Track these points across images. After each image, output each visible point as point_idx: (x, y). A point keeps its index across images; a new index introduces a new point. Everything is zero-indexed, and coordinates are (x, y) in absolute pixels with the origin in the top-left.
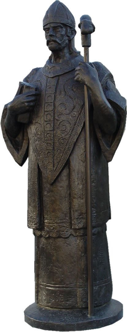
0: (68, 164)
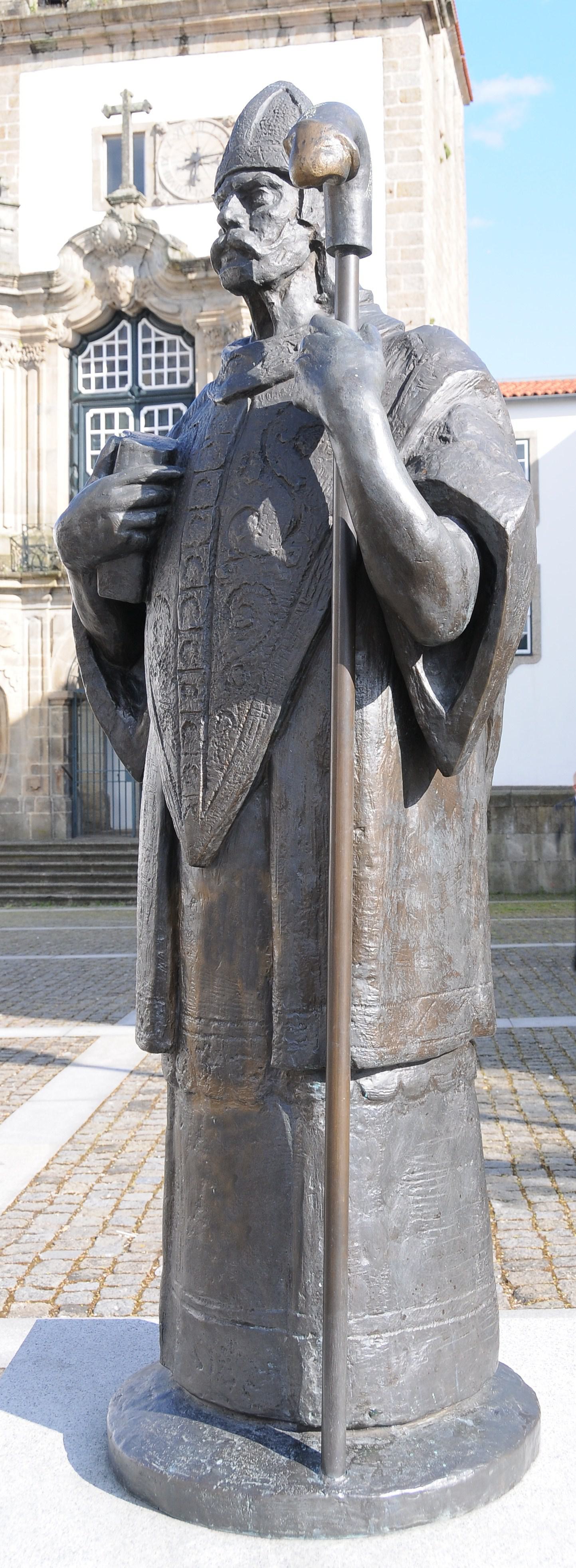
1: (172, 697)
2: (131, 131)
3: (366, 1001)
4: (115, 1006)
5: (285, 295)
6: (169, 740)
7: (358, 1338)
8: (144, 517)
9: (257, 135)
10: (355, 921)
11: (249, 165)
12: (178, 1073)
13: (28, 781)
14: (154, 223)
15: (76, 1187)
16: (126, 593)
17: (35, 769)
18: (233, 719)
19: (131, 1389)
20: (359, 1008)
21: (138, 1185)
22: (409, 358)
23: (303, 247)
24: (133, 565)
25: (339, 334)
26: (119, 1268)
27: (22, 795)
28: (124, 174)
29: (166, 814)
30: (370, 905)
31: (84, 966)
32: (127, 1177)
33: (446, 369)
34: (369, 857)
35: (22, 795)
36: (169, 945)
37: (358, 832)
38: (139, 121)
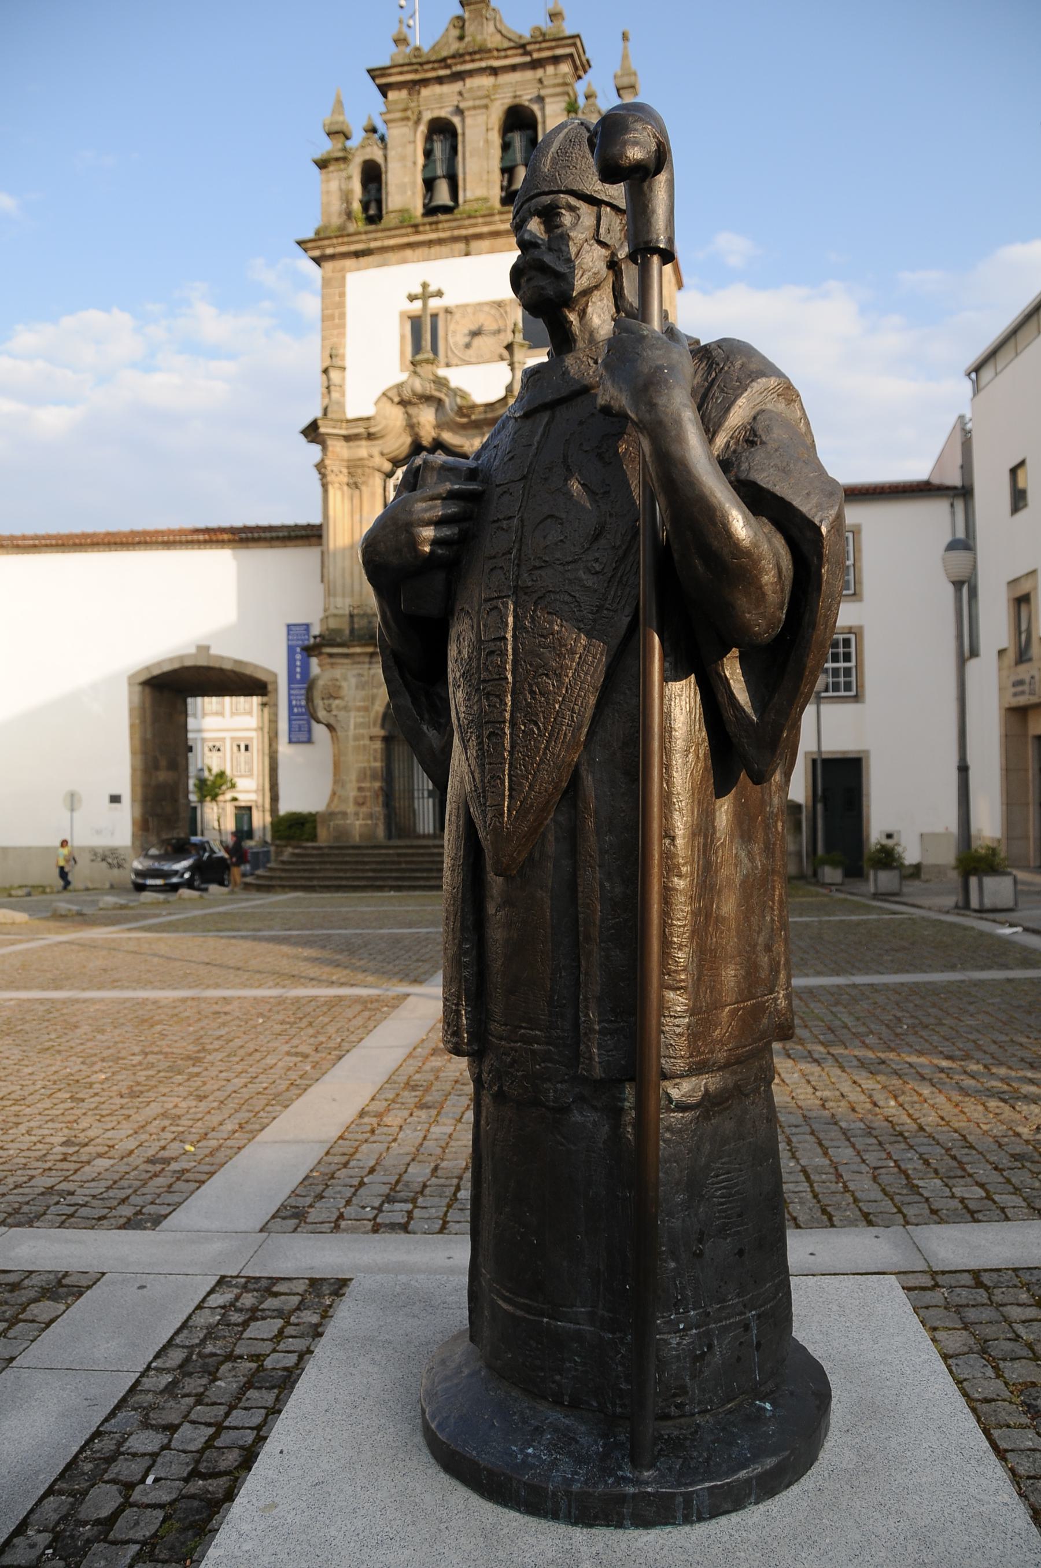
1: (475, 708)
2: (429, 312)
3: (676, 1011)
4: (421, 970)
5: (583, 315)
6: (472, 752)
7: (665, 1337)
9: (554, 162)
10: (664, 931)
11: (547, 189)
12: (485, 1076)
13: (355, 798)
14: (446, 379)
15: (393, 1119)
17: (360, 789)
18: (539, 728)
19: (443, 1362)
20: (668, 1019)
21: (442, 1119)
22: (710, 366)
23: (601, 267)
25: (645, 333)
26: (427, 1191)
27: (351, 809)
28: (423, 343)
29: (470, 823)
30: (680, 915)
31: (396, 940)
32: (434, 1112)
33: (750, 376)
34: (678, 866)
35: (351, 809)
36: (474, 952)
37: (667, 841)
38: (434, 303)
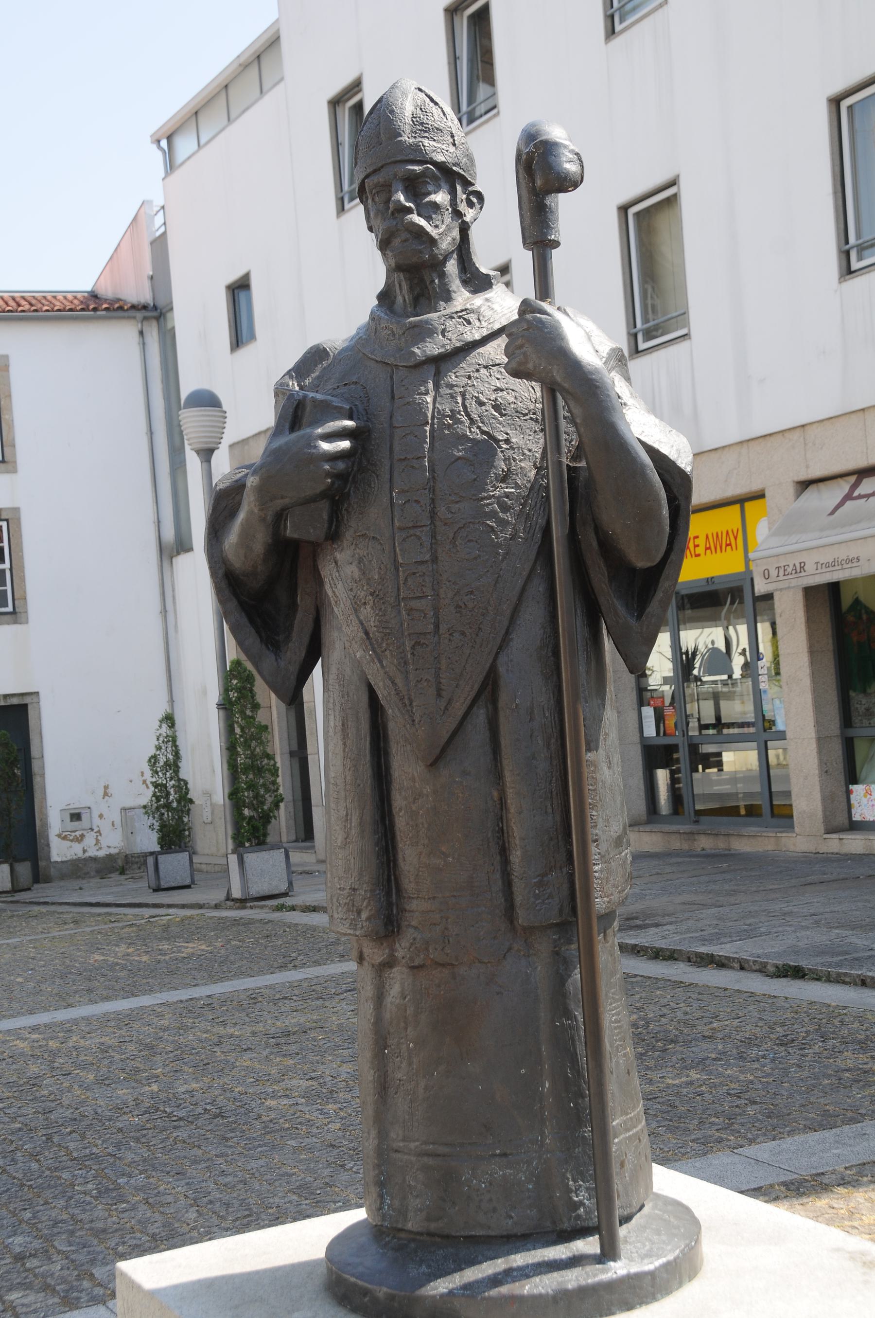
0: (490, 687)
8: (341, 465)
16: (315, 532)
24: (323, 509)
